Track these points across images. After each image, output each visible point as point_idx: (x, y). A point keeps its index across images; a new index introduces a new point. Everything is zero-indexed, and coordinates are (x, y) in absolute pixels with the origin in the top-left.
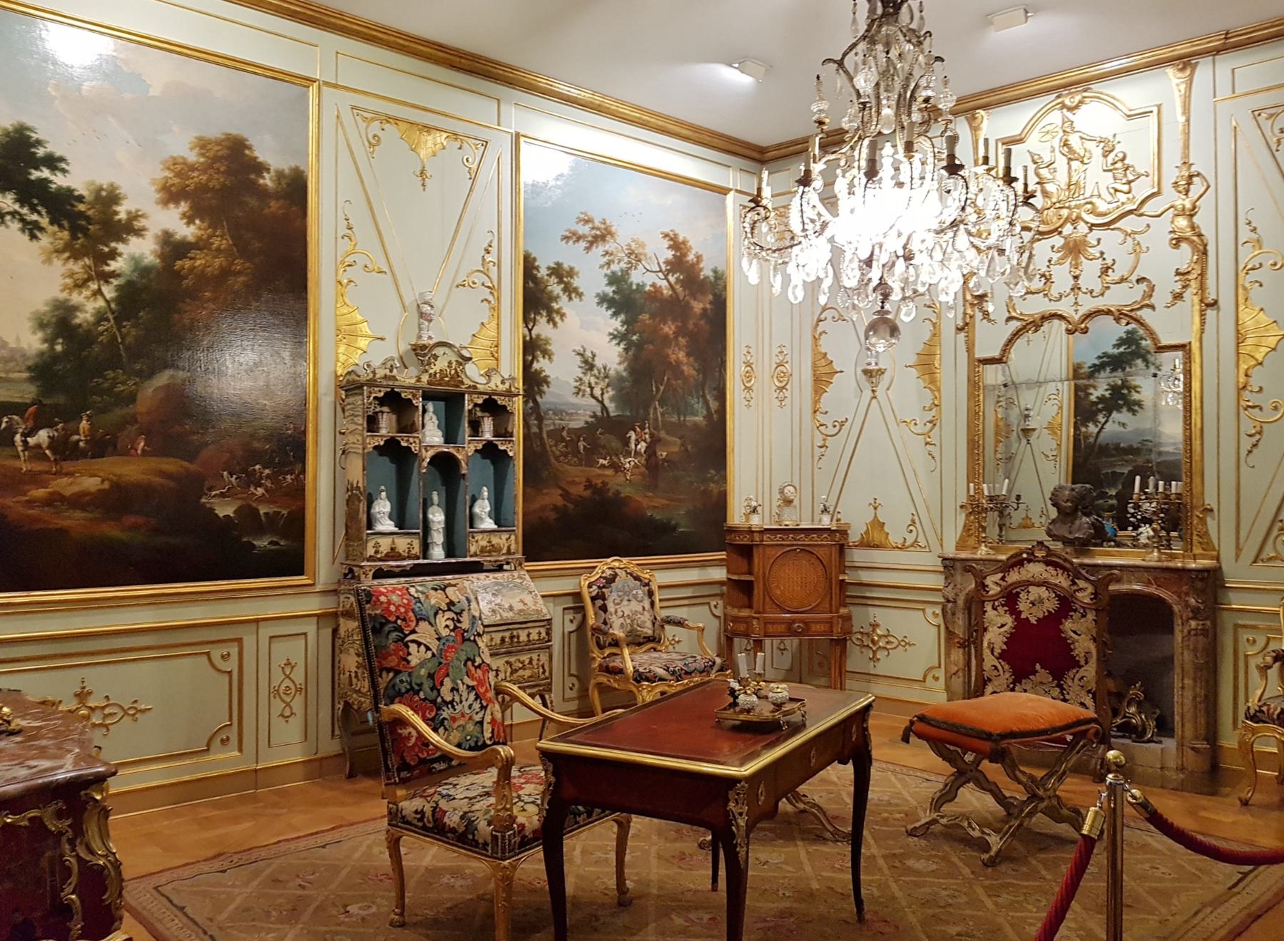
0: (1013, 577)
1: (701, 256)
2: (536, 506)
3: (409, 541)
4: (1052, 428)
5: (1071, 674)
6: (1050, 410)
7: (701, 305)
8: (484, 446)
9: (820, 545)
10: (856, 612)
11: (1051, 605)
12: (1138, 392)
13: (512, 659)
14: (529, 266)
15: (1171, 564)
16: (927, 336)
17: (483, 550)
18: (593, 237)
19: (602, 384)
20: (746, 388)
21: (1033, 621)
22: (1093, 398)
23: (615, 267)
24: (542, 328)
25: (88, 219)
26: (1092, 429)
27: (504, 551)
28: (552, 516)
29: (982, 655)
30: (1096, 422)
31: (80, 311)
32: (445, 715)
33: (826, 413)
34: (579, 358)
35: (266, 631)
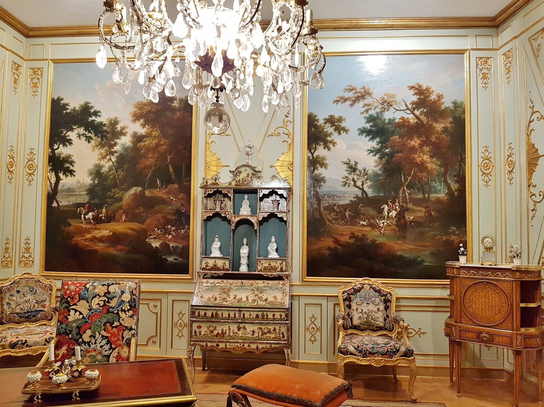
1: (442, 95)
2: (316, 247)
3: (224, 262)
7: (443, 125)
8: (268, 215)
9: (504, 281)
13: (263, 327)
14: (312, 120)
17: (265, 269)
18: (355, 98)
19: (362, 179)
20: (9, 171)
23: (372, 112)
24: (321, 151)
25: (107, 132)
27: (279, 270)
28: (327, 253)
34: (345, 166)
35: (171, 297)
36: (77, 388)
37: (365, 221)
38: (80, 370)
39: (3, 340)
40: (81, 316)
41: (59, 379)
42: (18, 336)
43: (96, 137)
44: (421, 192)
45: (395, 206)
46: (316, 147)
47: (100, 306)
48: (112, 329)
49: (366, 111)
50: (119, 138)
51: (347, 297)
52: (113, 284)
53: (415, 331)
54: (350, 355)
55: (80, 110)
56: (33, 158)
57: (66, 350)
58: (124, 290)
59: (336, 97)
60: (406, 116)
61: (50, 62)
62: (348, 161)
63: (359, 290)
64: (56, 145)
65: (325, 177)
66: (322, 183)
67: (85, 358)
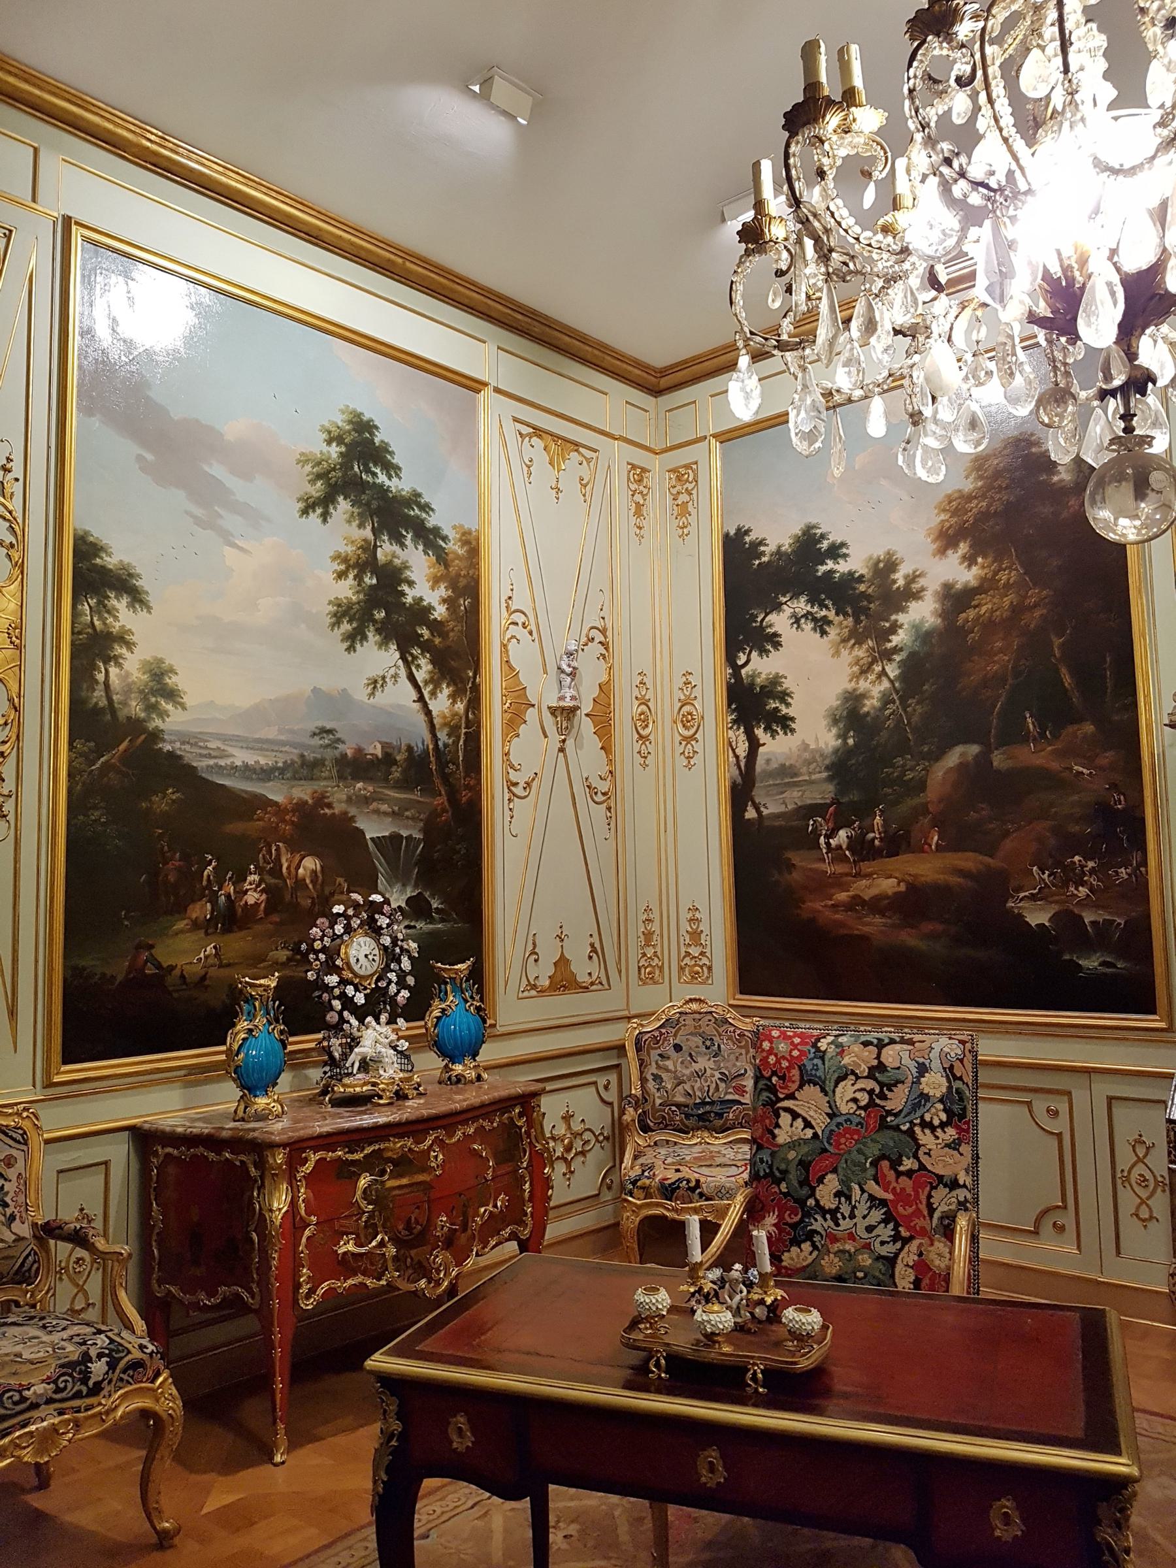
20: (641, 737)
31: (867, 698)
32: (816, 1226)
35: (1104, 1088)
36: (759, 1358)
38: (769, 1300)
39: (646, 1174)
40: (809, 1133)
41: (709, 1322)
42: (681, 1168)
43: (841, 617)
47: (859, 1108)
48: (897, 1178)
50: (903, 610)
52: (892, 1042)
55: (793, 551)
56: (693, 696)
57: (774, 1225)
58: (927, 1062)
61: (713, 441)
64: (741, 654)
67: (826, 1257)
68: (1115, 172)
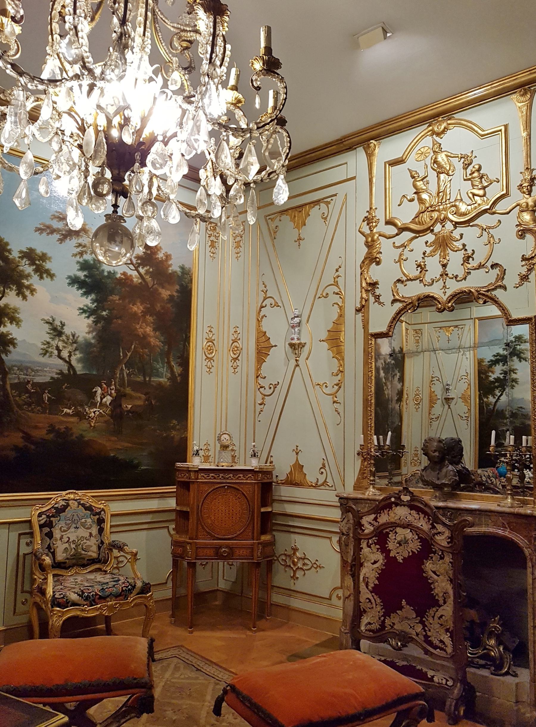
0: (384, 518)
1: (170, 255)
4: (465, 398)
5: (431, 612)
6: (462, 386)
7: (169, 293)
10: (280, 537)
11: (415, 546)
12: (516, 373)
15: (522, 511)
16: (335, 317)
19: (70, 348)
20: (208, 358)
21: (400, 559)
22: (491, 379)
26: (492, 399)
29: (359, 587)
30: (494, 395)
33: (265, 377)
34: (47, 326)
37: (70, 409)
44: (142, 374)
45: (111, 389)
46: (4, 291)
49: (79, 253)
51: (46, 521)
53: (127, 558)
54: (71, 606)
59: (40, 224)
60: (130, 272)
62: (51, 319)
63: (63, 509)
65: (16, 339)
66: (11, 348)
68: (508, 213)
